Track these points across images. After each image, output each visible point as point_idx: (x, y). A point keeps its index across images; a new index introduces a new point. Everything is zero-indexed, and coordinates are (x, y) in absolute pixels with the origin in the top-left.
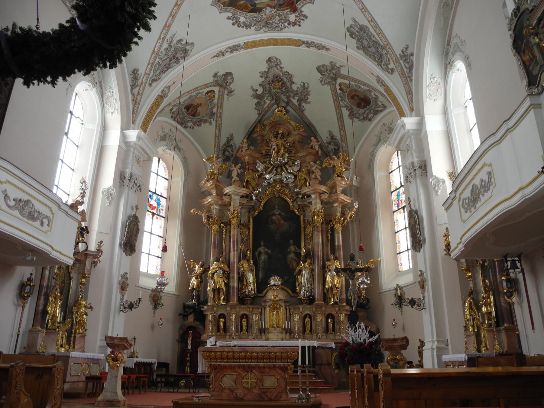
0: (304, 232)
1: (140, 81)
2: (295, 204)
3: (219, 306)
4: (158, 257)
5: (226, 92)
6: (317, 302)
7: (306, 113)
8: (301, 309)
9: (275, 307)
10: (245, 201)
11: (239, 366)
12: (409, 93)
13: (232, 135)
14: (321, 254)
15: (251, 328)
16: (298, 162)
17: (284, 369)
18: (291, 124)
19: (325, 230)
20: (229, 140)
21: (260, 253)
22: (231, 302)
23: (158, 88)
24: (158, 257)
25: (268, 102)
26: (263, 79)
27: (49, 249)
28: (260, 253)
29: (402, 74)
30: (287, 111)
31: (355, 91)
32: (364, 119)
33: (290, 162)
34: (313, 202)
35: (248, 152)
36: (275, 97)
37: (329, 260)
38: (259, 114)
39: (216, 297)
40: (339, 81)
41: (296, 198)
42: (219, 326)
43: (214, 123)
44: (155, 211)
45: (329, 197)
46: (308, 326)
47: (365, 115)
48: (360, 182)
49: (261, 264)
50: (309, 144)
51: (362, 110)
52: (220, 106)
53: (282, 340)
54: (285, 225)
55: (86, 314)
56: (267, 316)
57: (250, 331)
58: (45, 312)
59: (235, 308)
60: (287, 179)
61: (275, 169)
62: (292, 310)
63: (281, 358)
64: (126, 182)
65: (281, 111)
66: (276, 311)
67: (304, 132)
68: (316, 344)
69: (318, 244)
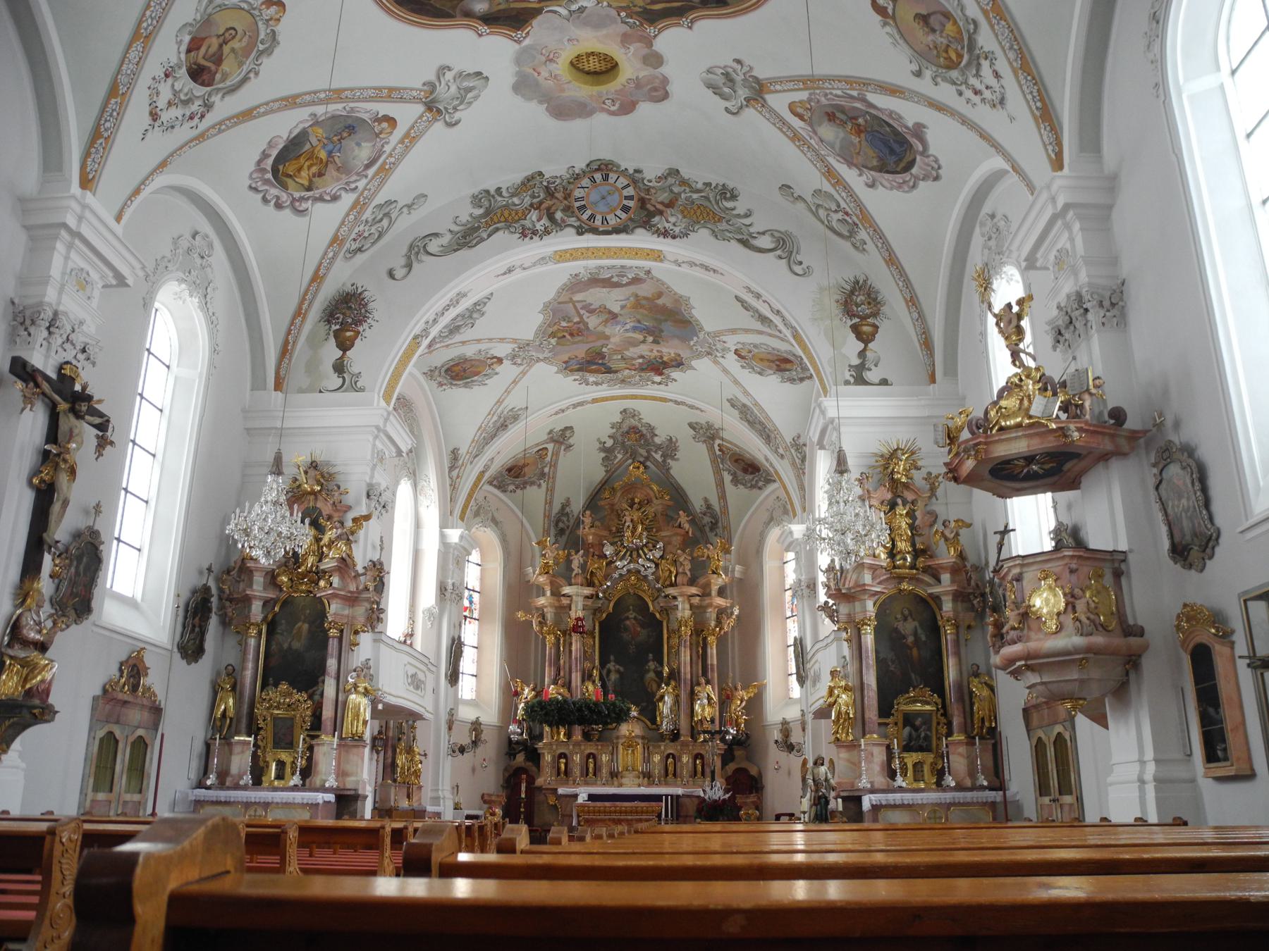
9: (630, 745)
10: (590, 602)
12: (802, 487)
13: (568, 500)
14: (689, 676)
16: (660, 545)
20: (563, 507)
25: (620, 456)
28: (609, 671)
29: (793, 464)
30: (646, 467)
32: (752, 487)
35: (593, 530)
37: (699, 684)
40: (718, 442)
42: (559, 769)
43: (544, 485)
44: (466, 613)
46: (671, 769)
48: (745, 573)
49: (610, 685)
52: (554, 465)
54: (643, 634)
56: (620, 756)
58: (394, 765)
64: (448, 595)
68: (680, 791)
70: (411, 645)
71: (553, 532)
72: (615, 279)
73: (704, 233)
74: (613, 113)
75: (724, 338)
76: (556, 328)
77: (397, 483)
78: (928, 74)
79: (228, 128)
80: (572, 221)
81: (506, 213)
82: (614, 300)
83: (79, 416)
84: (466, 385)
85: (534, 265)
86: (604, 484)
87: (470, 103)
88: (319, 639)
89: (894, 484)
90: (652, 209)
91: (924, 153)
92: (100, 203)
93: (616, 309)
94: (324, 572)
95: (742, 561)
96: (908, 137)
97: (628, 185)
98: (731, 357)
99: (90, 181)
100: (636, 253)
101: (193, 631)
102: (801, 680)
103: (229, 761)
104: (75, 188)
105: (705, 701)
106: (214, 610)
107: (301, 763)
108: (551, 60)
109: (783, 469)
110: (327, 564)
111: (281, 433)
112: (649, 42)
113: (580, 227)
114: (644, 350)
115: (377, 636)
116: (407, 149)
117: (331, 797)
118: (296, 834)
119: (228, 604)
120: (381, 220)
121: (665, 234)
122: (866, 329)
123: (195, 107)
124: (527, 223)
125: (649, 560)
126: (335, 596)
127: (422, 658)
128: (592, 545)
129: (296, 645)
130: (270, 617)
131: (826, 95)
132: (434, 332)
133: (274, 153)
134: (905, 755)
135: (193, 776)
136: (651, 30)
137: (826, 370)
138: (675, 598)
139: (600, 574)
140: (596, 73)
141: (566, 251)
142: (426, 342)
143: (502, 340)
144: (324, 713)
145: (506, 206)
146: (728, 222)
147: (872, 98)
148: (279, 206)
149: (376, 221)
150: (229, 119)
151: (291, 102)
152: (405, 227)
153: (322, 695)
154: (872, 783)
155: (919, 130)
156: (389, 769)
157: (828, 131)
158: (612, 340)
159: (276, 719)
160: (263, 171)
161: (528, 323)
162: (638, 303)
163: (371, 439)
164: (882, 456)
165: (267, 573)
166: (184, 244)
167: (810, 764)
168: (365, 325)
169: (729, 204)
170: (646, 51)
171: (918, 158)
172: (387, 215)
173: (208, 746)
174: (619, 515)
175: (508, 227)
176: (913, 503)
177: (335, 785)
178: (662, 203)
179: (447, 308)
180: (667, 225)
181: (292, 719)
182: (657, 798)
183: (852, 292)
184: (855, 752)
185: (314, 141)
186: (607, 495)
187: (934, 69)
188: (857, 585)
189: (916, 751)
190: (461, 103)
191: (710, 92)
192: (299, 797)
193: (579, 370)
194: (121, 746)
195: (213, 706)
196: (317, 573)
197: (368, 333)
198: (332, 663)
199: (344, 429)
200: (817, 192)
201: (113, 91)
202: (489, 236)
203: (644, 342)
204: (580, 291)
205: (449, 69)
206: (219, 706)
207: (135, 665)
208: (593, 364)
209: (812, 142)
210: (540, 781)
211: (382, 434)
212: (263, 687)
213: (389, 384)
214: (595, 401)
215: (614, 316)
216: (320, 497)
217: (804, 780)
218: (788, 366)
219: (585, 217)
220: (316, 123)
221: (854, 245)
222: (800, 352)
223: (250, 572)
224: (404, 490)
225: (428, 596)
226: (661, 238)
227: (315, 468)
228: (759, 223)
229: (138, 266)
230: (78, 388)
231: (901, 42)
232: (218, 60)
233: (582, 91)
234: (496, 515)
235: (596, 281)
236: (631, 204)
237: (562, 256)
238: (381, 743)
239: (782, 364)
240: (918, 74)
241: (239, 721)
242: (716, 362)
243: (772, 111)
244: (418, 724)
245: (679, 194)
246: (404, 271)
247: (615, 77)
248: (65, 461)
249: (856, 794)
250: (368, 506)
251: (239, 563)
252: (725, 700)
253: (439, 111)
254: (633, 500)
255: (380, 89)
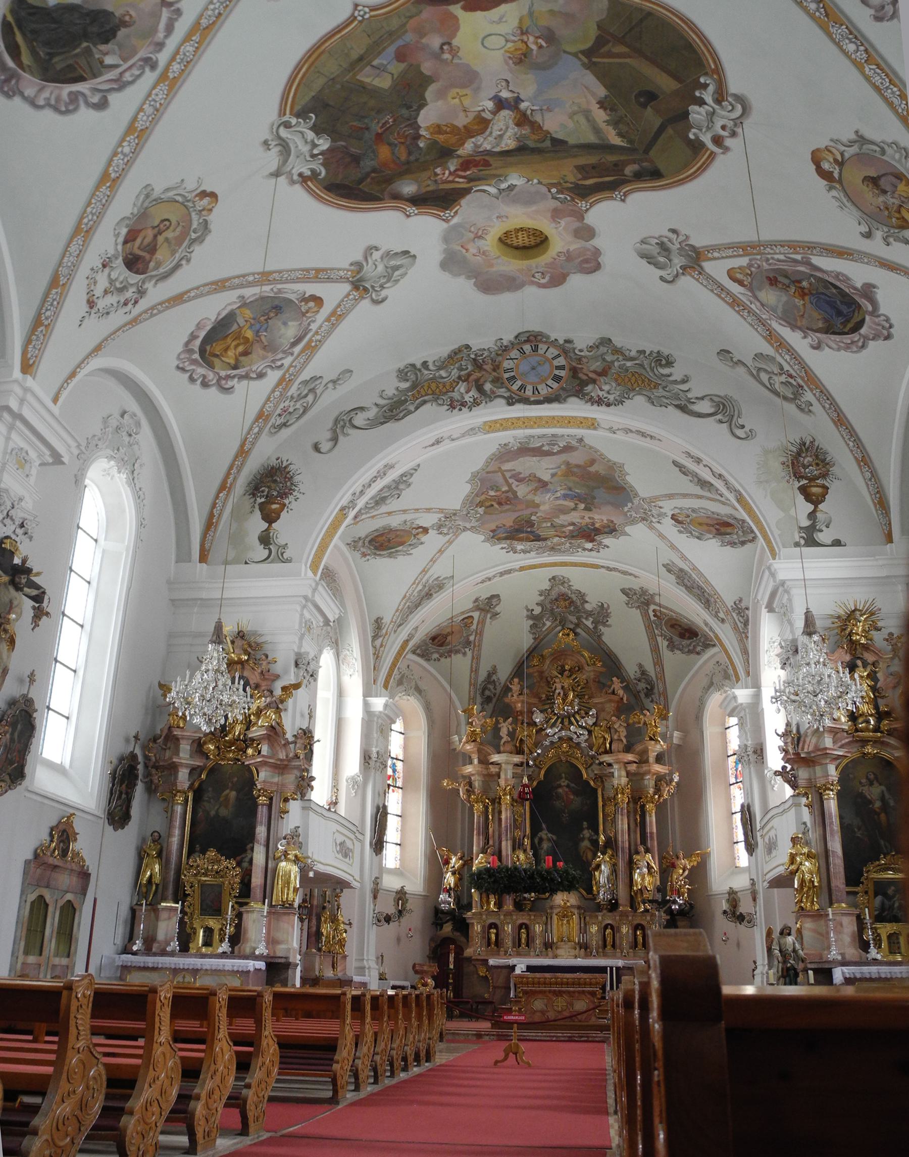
0: (603, 810)
1: (384, 631)
2: (590, 772)
3: (490, 913)
4: (397, 844)
5: (489, 616)
6: (621, 908)
7: (604, 638)
8: (600, 918)
9: (565, 914)
11: (550, 991)
12: (745, 652)
15: (533, 941)
16: (593, 712)
17: (593, 994)
18: (583, 656)
19: (632, 810)
20: (490, 675)
21: (541, 840)
22: (505, 907)
23: (403, 635)
24: (397, 844)
25: (548, 624)
26: (542, 598)
27: (351, 878)
28: (541, 840)
29: (735, 628)
30: (576, 634)
31: (677, 620)
32: (690, 652)
33: (582, 712)
34: (616, 774)
35: (521, 698)
36: (558, 618)
37: (637, 853)
38: (535, 639)
39: (484, 900)
40: (652, 607)
41: (591, 765)
42: (489, 939)
43: (469, 654)
44: (390, 782)
45: (638, 767)
46: (609, 940)
47: (691, 648)
50: (610, 687)
51: (688, 642)
52: (480, 633)
53: (576, 957)
54: (576, 802)
55: (346, 932)
56: (555, 927)
57: (531, 945)
58: (319, 934)
59: (511, 915)
60: (578, 737)
61: (560, 720)
62: (587, 918)
63: (591, 984)
64: (372, 763)
65: (568, 635)
66: (566, 919)
67: (602, 666)
69: (622, 831)
70: (335, 812)
71: (479, 699)
72: (546, 448)
73: (639, 400)
74: (544, 286)
75: (660, 504)
76: (483, 497)
77: (320, 652)
78: (879, 234)
79: (160, 312)
80: (502, 391)
81: (433, 386)
82: (544, 468)
83: (18, 588)
84: (390, 556)
85: (463, 435)
86: (532, 652)
87: (397, 281)
88: (247, 807)
89: (853, 646)
90: (585, 378)
91: (875, 312)
92: (39, 386)
93: (546, 477)
94: (252, 740)
95: (681, 726)
96: (857, 298)
97: (558, 356)
98: (668, 522)
99: (31, 365)
100: (569, 422)
101: (119, 797)
102: (751, 848)
103: (155, 928)
104: (17, 373)
105: (645, 870)
106: (140, 777)
107: (229, 930)
108: (480, 237)
109: (725, 634)
110: (255, 732)
111: (221, 602)
112: (580, 216)
113: (511, 397)
114: (575, 517)
115: (306, 804)
116: (334, 326)
117: (261, 965)
118: (271, 998)
119: (154, 771)
120: (306, 396)
121: (599, 402)
122: (815, 490)
123: (130, 294)
124: (455, 395)
125: (581, 727)
126: (264, 763)
127: (346, 823)
128: (522, 713)
129: (224, 812)
130: (196, 785)
131: (768, 260)
132: (361, 503)
133: (202, 334)
134: (878, 925)
135: (119, 941)
136: (582, 205)
137: (775, 533)
138: (610, 765)
139: (529, 742)
140: (525, 248)
141: (496, 422)
142: (352, 514)
143: (428, 510)
144: (253, 880)
145: (433, 379)
146: (664, 388)
147: (817, 261)
148: (205, 384)
149: (301, 397)
150: (161, 304)
151: (220, 285)
152: (330, 402)
153: (251, 861)
154: (843, 955)
155: (868, 291)
156: (314, 938)
157: (770, 296)
158: (542, 508)
159: (203, 885)
160: (191, 351)
161: (455, 493)
162: (570, 470)
163: (299, 609)
164: (839, 617)
165: (194, 741)
166: (113, 423)
167: (776, 935)
168: (291, 498)
169: (666, 371)
170: (577, 224)
171: (867, 318)
172: (312, 390)
173: (133, 912)
174: (548, 682)
175: (436, 400)
176: (873, 664)
177: (266, 952)
178: (595, 372)
179: (374, 480)
180: (601, 393)
181: (220, 886)
182: (602, 970)
183: (799, 454)
184: (822, 922)
185: (241, 322)
186: (535, 662)
187: (886, 229)
188: (817, 749)
189: (890, 921)
190: (388, 281)
191: (644, 262)
192: (229, 964)
193: (506, 538)
194: (51, 909)
195: (138, 872)
196: (245, 741)
197: (294, 505)
198: (261, 831)
199: (272, 599)
200: (759, 356)
201: (54, 282)
202: (417, 408)
203: (575, 509)
204: (508, 461)
205: (377, 249)
206: (145, 872)
207: (64, 831)
208: (522, 532)
209: (753, 306)
210: (468, 952)
211: (309, 604)
212: (189, 855)
213: (315, 555)
214: (522, 569)
215: (543, 485)
216: (246, 666)
217: (769, 950)
218: (729, 530)
219: (515, 387)
220: (244, 305)
221: (799, 407)
222: (743, 515)
223: (177, 740)
224: (327, 659)
225: (352, 765)
226: (595, 407)
227: (242, 637)
228: (696, 389)
229: (73, 444)
230: (17, 561)
231: (848, 204)
232: (152, 249)
233: (511, 265)
234: (419, 683)
235: (525, 450)
236: (562, 373)
237: (491, 427)
238: (305, 912)
239: (722, 528)
240: (868, 235)
241: (165, 888)
242: (651, 528)
243: (709, 277)
244: (346, 895)
245: (613, 362)
246: (330, 444)
247: (545, 250)
248: (6, 631)
249: (827, 966)
250: (297, 675)
251: (166, 731)
252: (667, 869)
253: (366, 290)
254: (563, 667)
255: (307, 270)
